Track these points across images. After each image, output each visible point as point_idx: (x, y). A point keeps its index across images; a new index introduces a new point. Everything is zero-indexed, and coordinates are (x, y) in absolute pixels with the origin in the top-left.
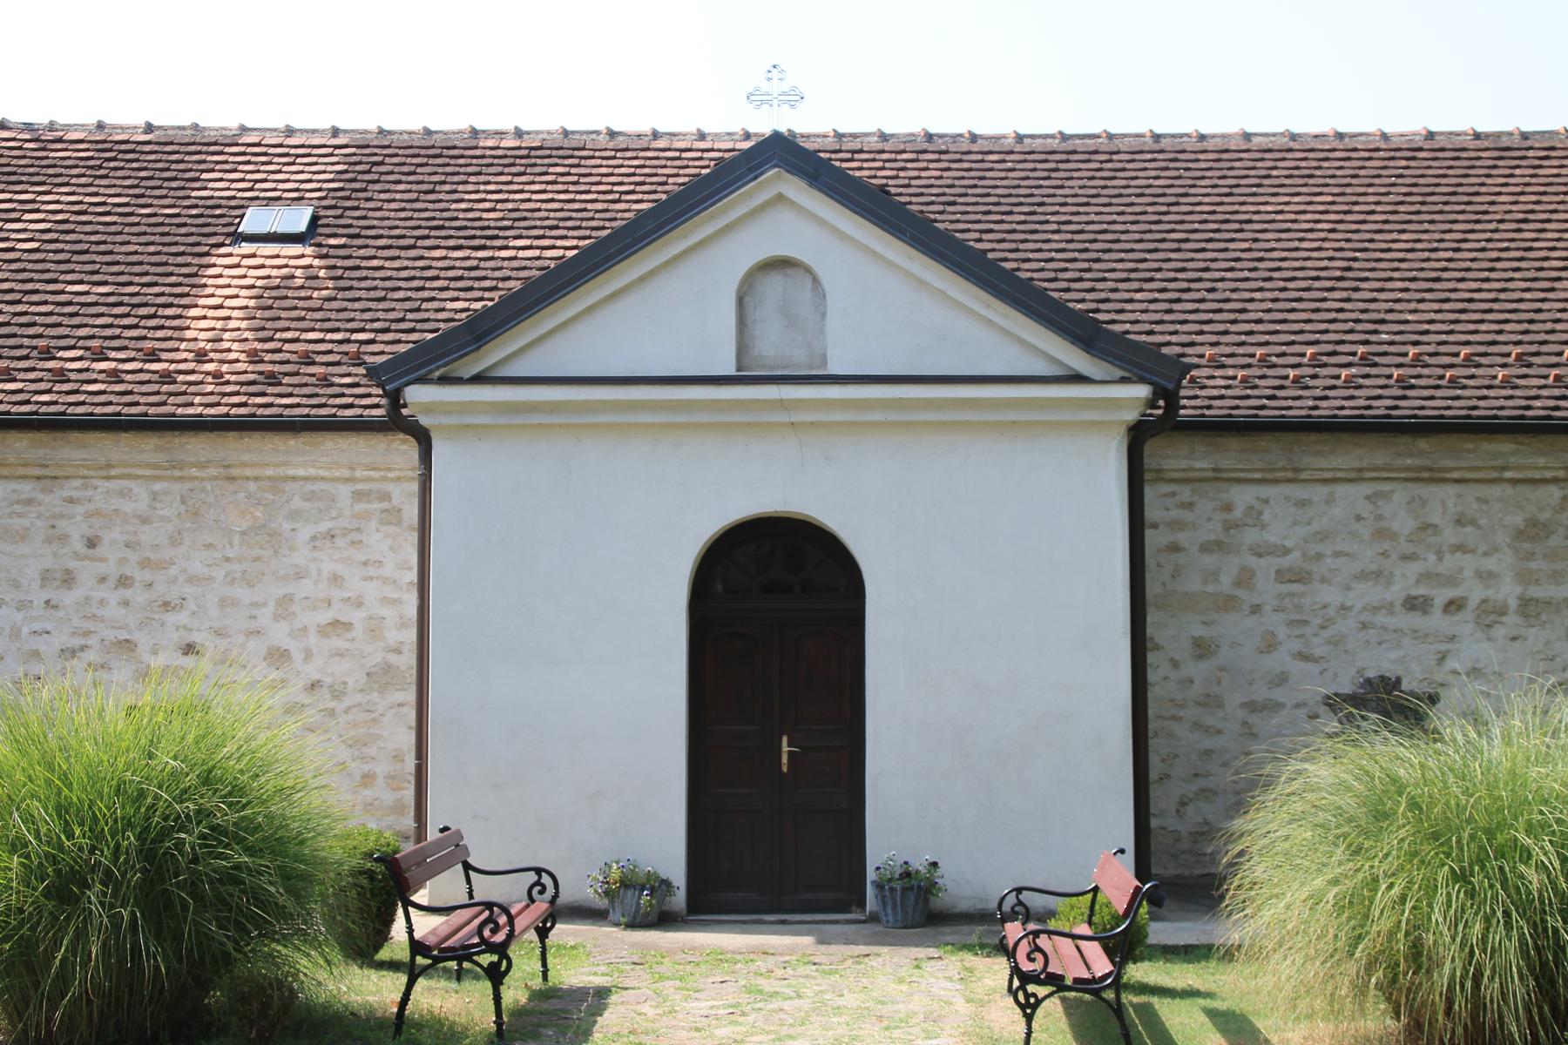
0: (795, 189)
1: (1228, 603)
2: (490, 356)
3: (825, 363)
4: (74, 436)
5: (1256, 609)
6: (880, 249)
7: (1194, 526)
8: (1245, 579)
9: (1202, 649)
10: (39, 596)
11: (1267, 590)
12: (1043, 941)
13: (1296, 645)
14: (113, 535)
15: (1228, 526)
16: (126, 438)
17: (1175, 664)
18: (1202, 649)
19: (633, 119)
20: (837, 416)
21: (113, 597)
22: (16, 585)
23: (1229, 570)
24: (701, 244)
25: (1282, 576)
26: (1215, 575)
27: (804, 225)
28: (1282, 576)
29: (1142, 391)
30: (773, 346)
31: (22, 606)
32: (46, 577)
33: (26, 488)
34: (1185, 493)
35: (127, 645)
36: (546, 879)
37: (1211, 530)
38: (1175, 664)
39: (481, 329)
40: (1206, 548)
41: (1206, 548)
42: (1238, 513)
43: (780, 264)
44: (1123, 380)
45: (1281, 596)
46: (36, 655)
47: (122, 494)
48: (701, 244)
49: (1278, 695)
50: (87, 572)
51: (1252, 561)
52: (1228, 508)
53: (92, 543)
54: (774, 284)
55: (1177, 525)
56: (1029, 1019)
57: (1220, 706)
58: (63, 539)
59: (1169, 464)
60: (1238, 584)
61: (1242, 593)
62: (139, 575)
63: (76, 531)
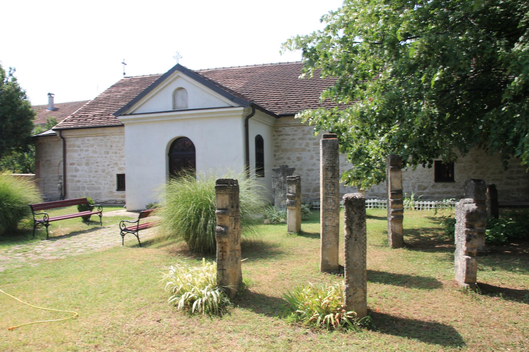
1: (304, 150)
2: (132, 110)
5: (309, 151)
7: (297, 135)
8: (307, 145)
12: (125, 223)
15: (304, 134)
16: (114, 128)
17: (294, 162)
18: (299, 159)
19: (227, 65)
20: (203, 116)
23: (304, 143)
24: (166, 86)
26: (300, 145)
27: (184, 81)
30: (180, 104)
31: (102, 157)
32: (105, 152)
33: (102, 138)
34: (295, 128)
35: (116, 164)
36: (46, 216)
37: (300, 136)
39: (129, 105)
40: (300, 139)
41: (300, 139)
42: (306, 132)
43: (181, 89)
44: (240, 107)
45: (314, 148)
47: (115, 138)
52: (304, 131)
53: (111, 146)
54: (180, 93)
55: (294, 135)
58: (107, 146)
59: (291, 123)
60: (306, 146)
62: (118, 152)
63: (109, 144)
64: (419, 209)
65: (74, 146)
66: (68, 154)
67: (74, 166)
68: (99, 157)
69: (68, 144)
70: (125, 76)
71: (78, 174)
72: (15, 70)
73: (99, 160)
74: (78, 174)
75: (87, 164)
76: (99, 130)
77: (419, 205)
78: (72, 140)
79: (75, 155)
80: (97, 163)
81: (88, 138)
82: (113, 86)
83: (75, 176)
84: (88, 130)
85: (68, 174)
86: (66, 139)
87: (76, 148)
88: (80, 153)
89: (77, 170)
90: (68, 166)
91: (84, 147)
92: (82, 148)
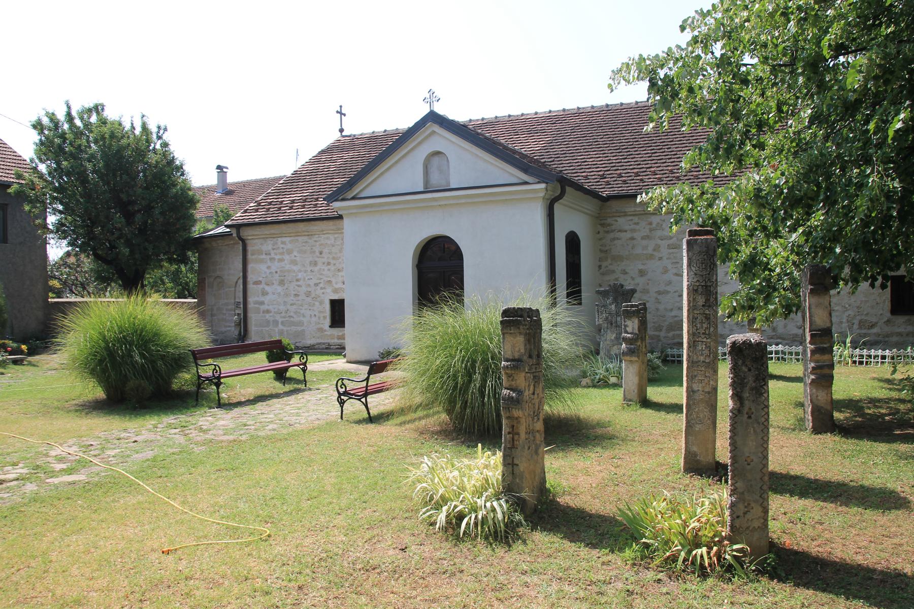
0: (436, 128)
1: (651, 257)
3: (449, 184)
4: (313, 223)
5: (660, 259)
6: (409, 148)
8: (657, 248)
9: (642, 273)
10: (309, 269)
11: (664, 252)
13: (675, 271)
14: (326, 251)
15: (651, 230)
17: (633, 279)
18: (642, 273)
20: (452, 202)
21: (326, 268)
22: (304, 266)
23: (651, 244)
24: (413, 149)
25: (670, 247)
27: (444, 141)
28: (670, 247)
29: (543, 186)
30: (436, 180)
32: (311, 263)
33: (305, 238)
34: (636, 219)
35: (330, 282)
38: (633, 279)
39: (351, 184)
40: (643, 238)
41: (643, 238)
42: (654, 226)
43: (438, 153)
44: (539, 183)
46: (309, 285)
47: (328, 238)
48: (413, 149)
49: (668, 288)
50: (320, 261)
51: (660, 242)
52: (651, 224)
53: (321, 253)
54: (436, 161)
55: (633, 231)
56: (342, 407)
57: (648, 292)
58: (314, 252)
60: (654, 250)
61: (655, 253)
62: (332, 262)
63: (317, 250)
64: (861, 363)
65: (260, 252)
66: (250, 267)
67: (261, 287)
68: (300, 271)
69: (250, 249)
70: (344, 134)
71: (266, 299)
72: (166, 130)
73: (300, 275)
74: (266, 299)
75: (282, 283)
76: (301, 226)
77: (862, 356)
78: (259, 243)
79: (263, 267)
80: (297, 280)
81: (284, 239)
82: (322, 152)
83: (262, 303)
84: (283, 226)
85: (251, 300)
86: (247, 242)
87: (264, 256)
88: (269, 264)
89: (265, 293)
90: (250, 286)
91: (276, 254)
92: (273, 255)
